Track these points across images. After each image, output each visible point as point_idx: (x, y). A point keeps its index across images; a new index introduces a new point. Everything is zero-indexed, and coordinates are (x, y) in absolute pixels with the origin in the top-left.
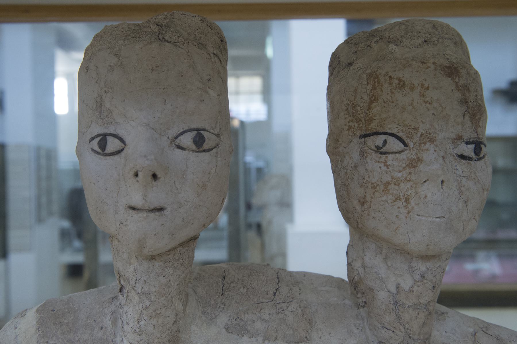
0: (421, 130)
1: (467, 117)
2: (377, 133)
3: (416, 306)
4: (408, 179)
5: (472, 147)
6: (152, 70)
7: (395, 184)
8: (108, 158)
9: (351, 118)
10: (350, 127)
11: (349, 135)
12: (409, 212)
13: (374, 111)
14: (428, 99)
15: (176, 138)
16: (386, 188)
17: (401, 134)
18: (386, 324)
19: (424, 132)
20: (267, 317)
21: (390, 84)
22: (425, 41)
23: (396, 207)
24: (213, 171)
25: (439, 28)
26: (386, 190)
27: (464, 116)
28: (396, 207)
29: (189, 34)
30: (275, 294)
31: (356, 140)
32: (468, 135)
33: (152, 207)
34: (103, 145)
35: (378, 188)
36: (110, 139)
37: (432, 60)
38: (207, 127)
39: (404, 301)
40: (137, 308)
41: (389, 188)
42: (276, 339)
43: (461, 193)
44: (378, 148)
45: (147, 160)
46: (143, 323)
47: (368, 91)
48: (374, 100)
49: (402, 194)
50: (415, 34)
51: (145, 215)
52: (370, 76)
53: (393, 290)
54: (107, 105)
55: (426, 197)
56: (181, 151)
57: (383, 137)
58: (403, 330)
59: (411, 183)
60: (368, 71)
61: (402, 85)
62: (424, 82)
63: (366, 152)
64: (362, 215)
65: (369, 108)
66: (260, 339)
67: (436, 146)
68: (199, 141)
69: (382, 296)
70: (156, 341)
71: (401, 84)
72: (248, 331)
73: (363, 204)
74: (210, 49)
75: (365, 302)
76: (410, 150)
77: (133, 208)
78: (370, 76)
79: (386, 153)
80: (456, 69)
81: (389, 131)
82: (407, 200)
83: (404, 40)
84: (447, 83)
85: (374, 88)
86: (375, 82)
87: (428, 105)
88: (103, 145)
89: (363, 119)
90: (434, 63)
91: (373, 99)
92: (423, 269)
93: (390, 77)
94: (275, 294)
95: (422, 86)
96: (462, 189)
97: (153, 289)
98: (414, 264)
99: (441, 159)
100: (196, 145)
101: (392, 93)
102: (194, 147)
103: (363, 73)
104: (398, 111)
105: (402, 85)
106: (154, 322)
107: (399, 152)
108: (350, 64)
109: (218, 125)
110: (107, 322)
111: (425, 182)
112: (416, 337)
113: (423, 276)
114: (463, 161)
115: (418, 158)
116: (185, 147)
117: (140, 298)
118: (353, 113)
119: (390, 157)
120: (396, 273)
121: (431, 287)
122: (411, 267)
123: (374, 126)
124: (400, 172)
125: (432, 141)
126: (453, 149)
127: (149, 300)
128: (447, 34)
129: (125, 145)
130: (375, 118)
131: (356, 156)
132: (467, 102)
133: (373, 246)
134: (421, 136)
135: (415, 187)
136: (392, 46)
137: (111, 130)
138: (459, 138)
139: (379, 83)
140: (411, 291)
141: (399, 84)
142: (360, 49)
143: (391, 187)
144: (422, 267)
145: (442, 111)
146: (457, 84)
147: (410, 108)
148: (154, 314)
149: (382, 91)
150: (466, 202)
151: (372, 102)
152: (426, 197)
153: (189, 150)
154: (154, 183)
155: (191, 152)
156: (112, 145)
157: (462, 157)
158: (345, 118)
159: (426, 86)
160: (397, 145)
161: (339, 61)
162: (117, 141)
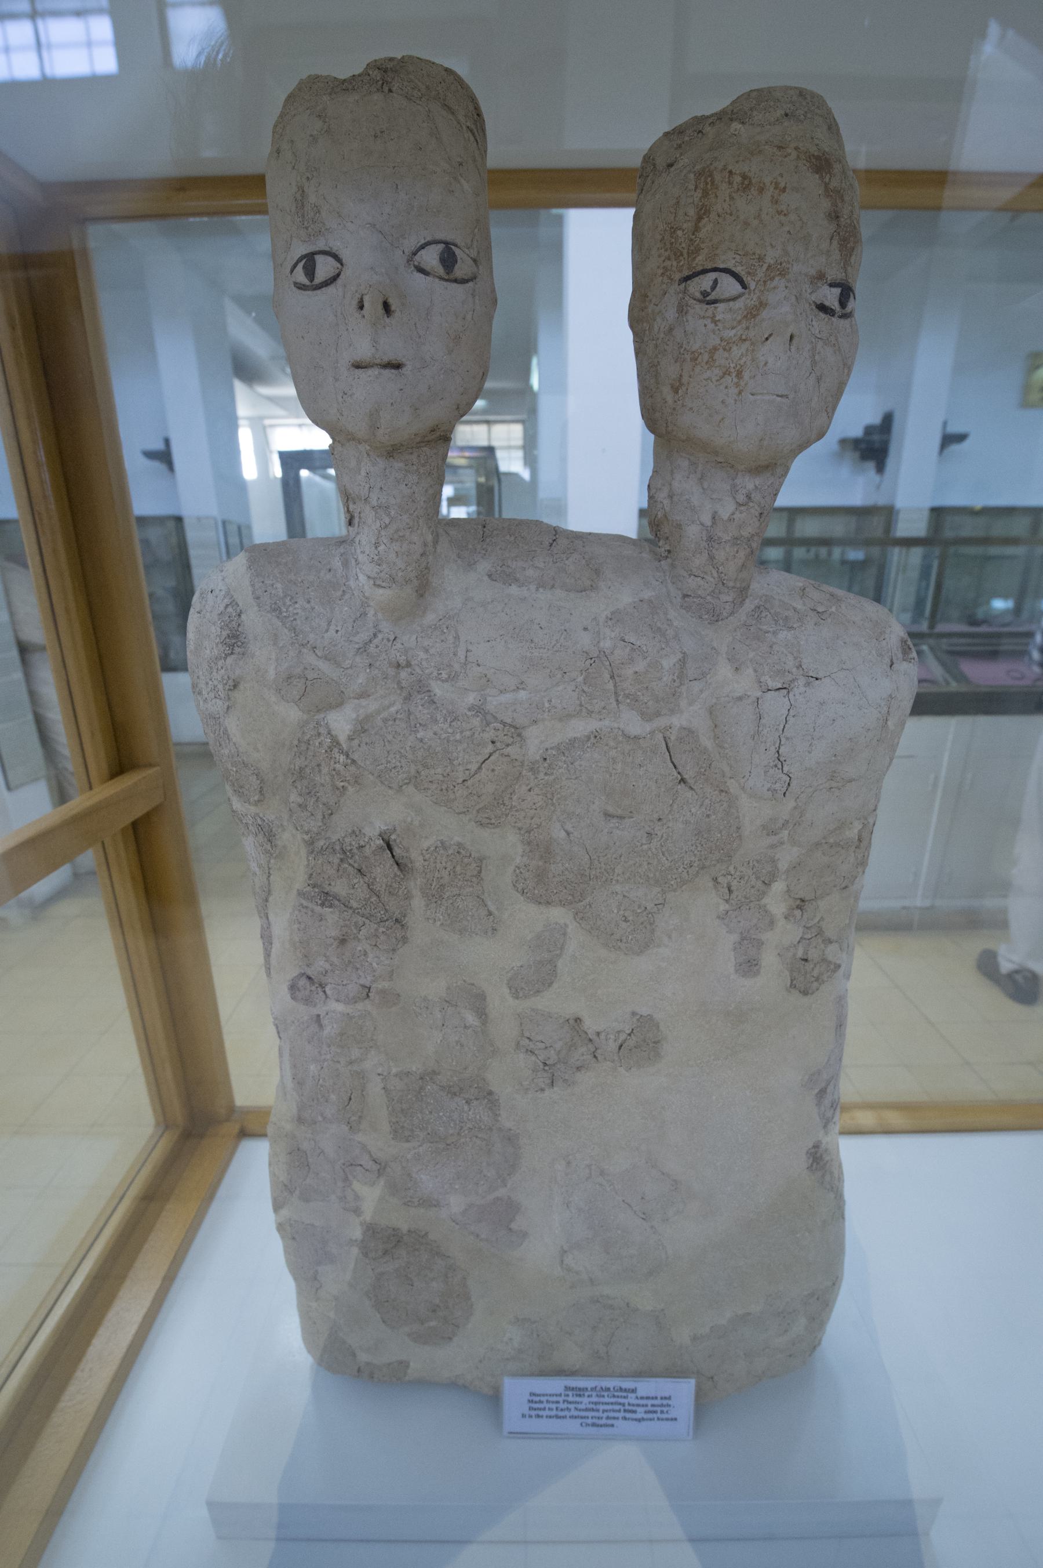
0: (769, 260)
1: (835, 242)
2: (704, 272)
3: (736, 540)
4: (744, 337)
5: (837, 291)
6: (376, 137)
7: (725, 350)
8: (319, 292)
9: (667, 254)
10: (665, 269)
11: (662, 283)
12: (740, 393)
13: (702, 234)
14: (783, 207)
15: (415, 254)
16: (712, 357)
17: (738, 269)
18: (694, 570)
19: (772, 262)
20: (542, 565)
21: (730, 183)
22: (787, 115)
23: (722, 387)
24: (469, 317)
25: (808, 97)
26: (711, 362)
27: (831, 239)
28: (722, 387)
29: (428, 87)
30: (551, 545)
31: (675, 287)
32: (834, 273)
33: (386, 359)
34: (310, 271)
35: (699, 360)
36: (320, 259)
37: (793, 145)
38: (458, 241)
39: (720, 534)
40: (374, 528)
41: (716, 357)
42: (553, 586)
43: (814, 363)
44: (705, 294)
45: (376, 273)
46: (382, 548)
47: (696, 200)
48: (704, 214)
49: (732, 365)
50: (772, 103)
51: (376, 373)
52: (699, 174)
53: (708, 522)
54: (312, 199)
55: (766, 364)
56: (422, 275)
57: (713, 275)
58: (715, 575)
59: (748, 343)
60: (698, 167)
61: (746, 184)
62: (780, 179)
63: (687, 305)
64: (674, 409)
65: (696, 229)
66: (533, 587)
67: (789, 281)
68: (448, 260)
69: (693, 532)
70: (400, 574)
71: (746, 182)
72: (517, 580)
73: (676, 391)
74: (462, 119)
75: (669, 551)
76: (749, 294)
77: (358, 366)
78: (699, 174)
79: (715, 302)
80: (827, 160)
81: (722, 266)
82: (739, 374)
83: (755, 113)
84: (812, 181)
85: (705, 194)
86: (707, 184)
87: (782, 218)
88: (310, 271)
89: (685, 252)
90: (796, 148)
91: (703, 212)
92: (750, 486)
93: (730, 172)
94: (551, 545)
95: (777, 184)
96: (817, 357)
97: (393, 501)
98: (738, 481)
99: (794, 298)
100: (444, 266)
101: (732, 198)
102: (441, 271)
103: (690, 172)
104: (738, 227)
105: (746, 184)
106: (396, 546)
107: (734, 299)
108: (670, 165)
109: (475, 243)
110: (337, 563)
111: (767, 339)
112: (731, 584)
113: (749, 497)
114: (822, 315)
115: (761, 303)
116: (428, 268)
117: (376, 513)
118: (672, 244)
119: (721, 307)
120: (714, 496)
121: (757, 514)
122: (734, 486)
123: (701, 261)
124: (733, 328)
125: (783, 273)
126: (810, 294)
127: (389, 515)
128: (818, 107)
129: (342, 264)
130: (702, 246)
131: (671, 314)
132: (838, 217)
133: (686, 463)
134: (767, 269)
135: (753, 350)
136: (736, 126)
137: (321, 245)
138: (821, 276)
139: (713, 182)
140: (730, 520)
141: (743, 183)
142: (687, 138)
143: (720, 355)
144: (749, 483)
145: (802, 227)
146: (826, 185)
147: (756, 222)
148: (396, 537)
149: (717, 196)
150: (819, 380)
151: (700, 218)
152: (766, 364)
153: (435, 276)
154: (387, 320)
155: (437, 280)
156: (324, 268)
157: (822, 308)
158: (659, 256)
159: (782, 185)
160: (735, 288)
161: (654, 165)
162: (330, 260)
